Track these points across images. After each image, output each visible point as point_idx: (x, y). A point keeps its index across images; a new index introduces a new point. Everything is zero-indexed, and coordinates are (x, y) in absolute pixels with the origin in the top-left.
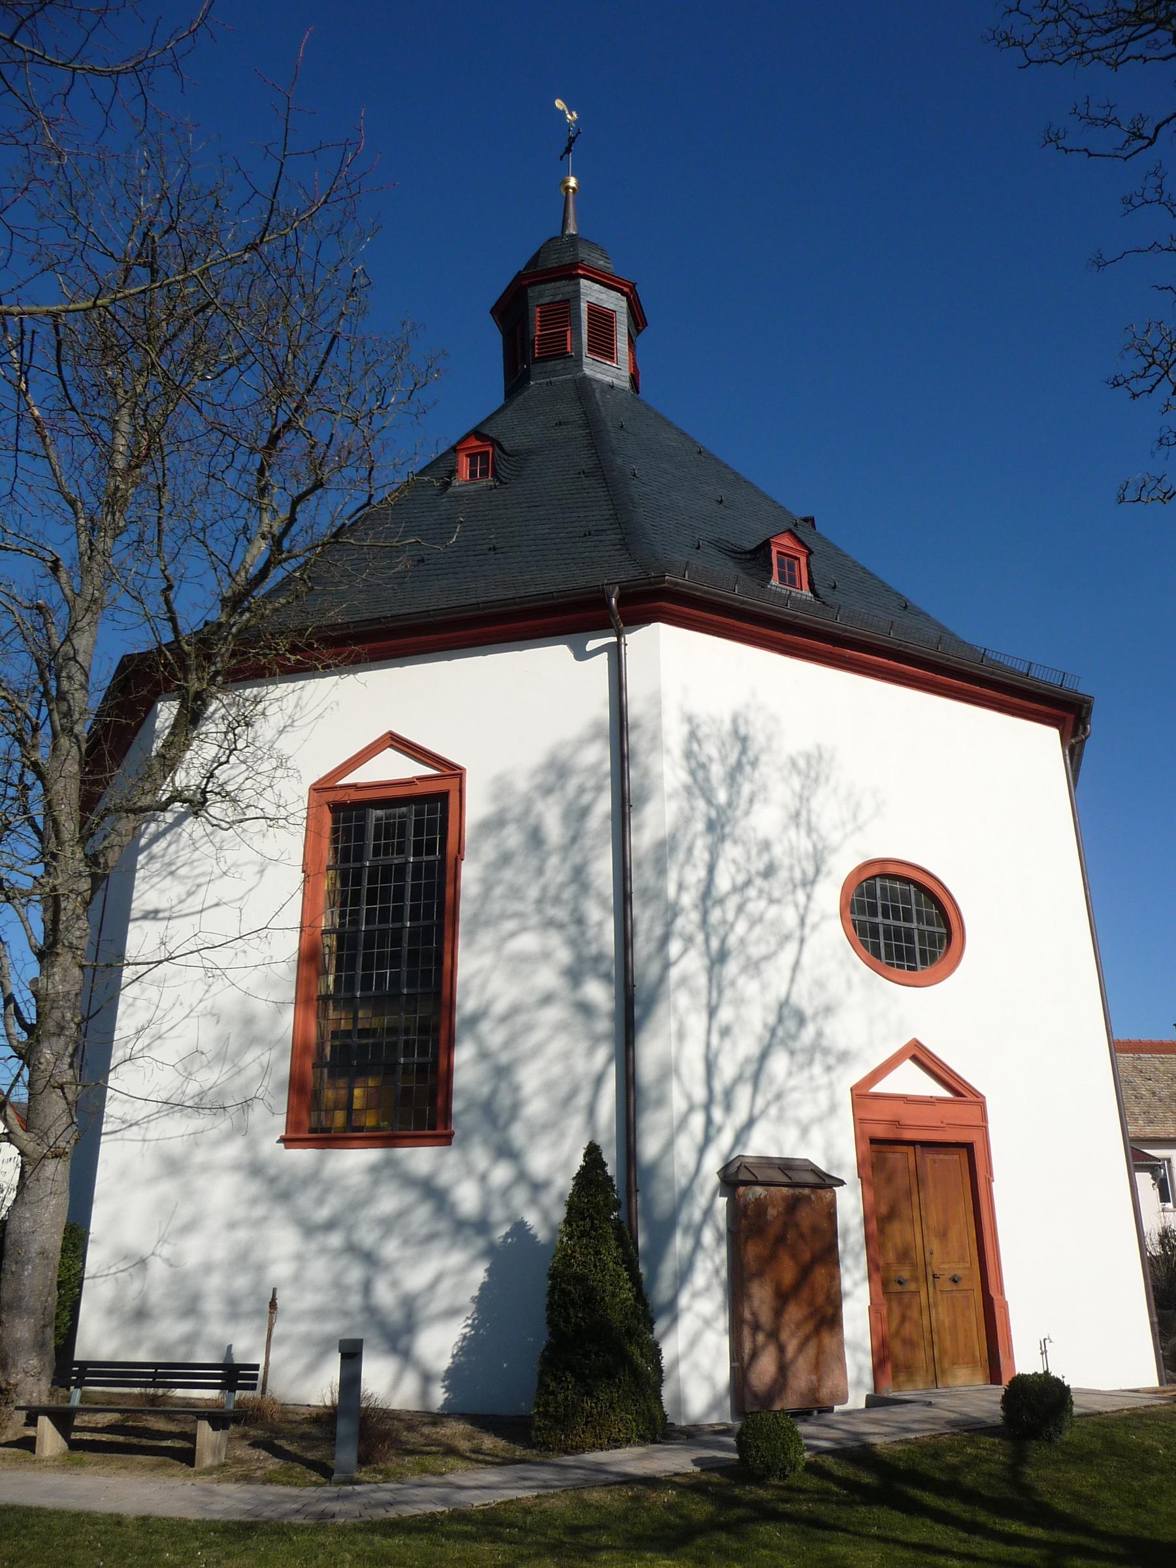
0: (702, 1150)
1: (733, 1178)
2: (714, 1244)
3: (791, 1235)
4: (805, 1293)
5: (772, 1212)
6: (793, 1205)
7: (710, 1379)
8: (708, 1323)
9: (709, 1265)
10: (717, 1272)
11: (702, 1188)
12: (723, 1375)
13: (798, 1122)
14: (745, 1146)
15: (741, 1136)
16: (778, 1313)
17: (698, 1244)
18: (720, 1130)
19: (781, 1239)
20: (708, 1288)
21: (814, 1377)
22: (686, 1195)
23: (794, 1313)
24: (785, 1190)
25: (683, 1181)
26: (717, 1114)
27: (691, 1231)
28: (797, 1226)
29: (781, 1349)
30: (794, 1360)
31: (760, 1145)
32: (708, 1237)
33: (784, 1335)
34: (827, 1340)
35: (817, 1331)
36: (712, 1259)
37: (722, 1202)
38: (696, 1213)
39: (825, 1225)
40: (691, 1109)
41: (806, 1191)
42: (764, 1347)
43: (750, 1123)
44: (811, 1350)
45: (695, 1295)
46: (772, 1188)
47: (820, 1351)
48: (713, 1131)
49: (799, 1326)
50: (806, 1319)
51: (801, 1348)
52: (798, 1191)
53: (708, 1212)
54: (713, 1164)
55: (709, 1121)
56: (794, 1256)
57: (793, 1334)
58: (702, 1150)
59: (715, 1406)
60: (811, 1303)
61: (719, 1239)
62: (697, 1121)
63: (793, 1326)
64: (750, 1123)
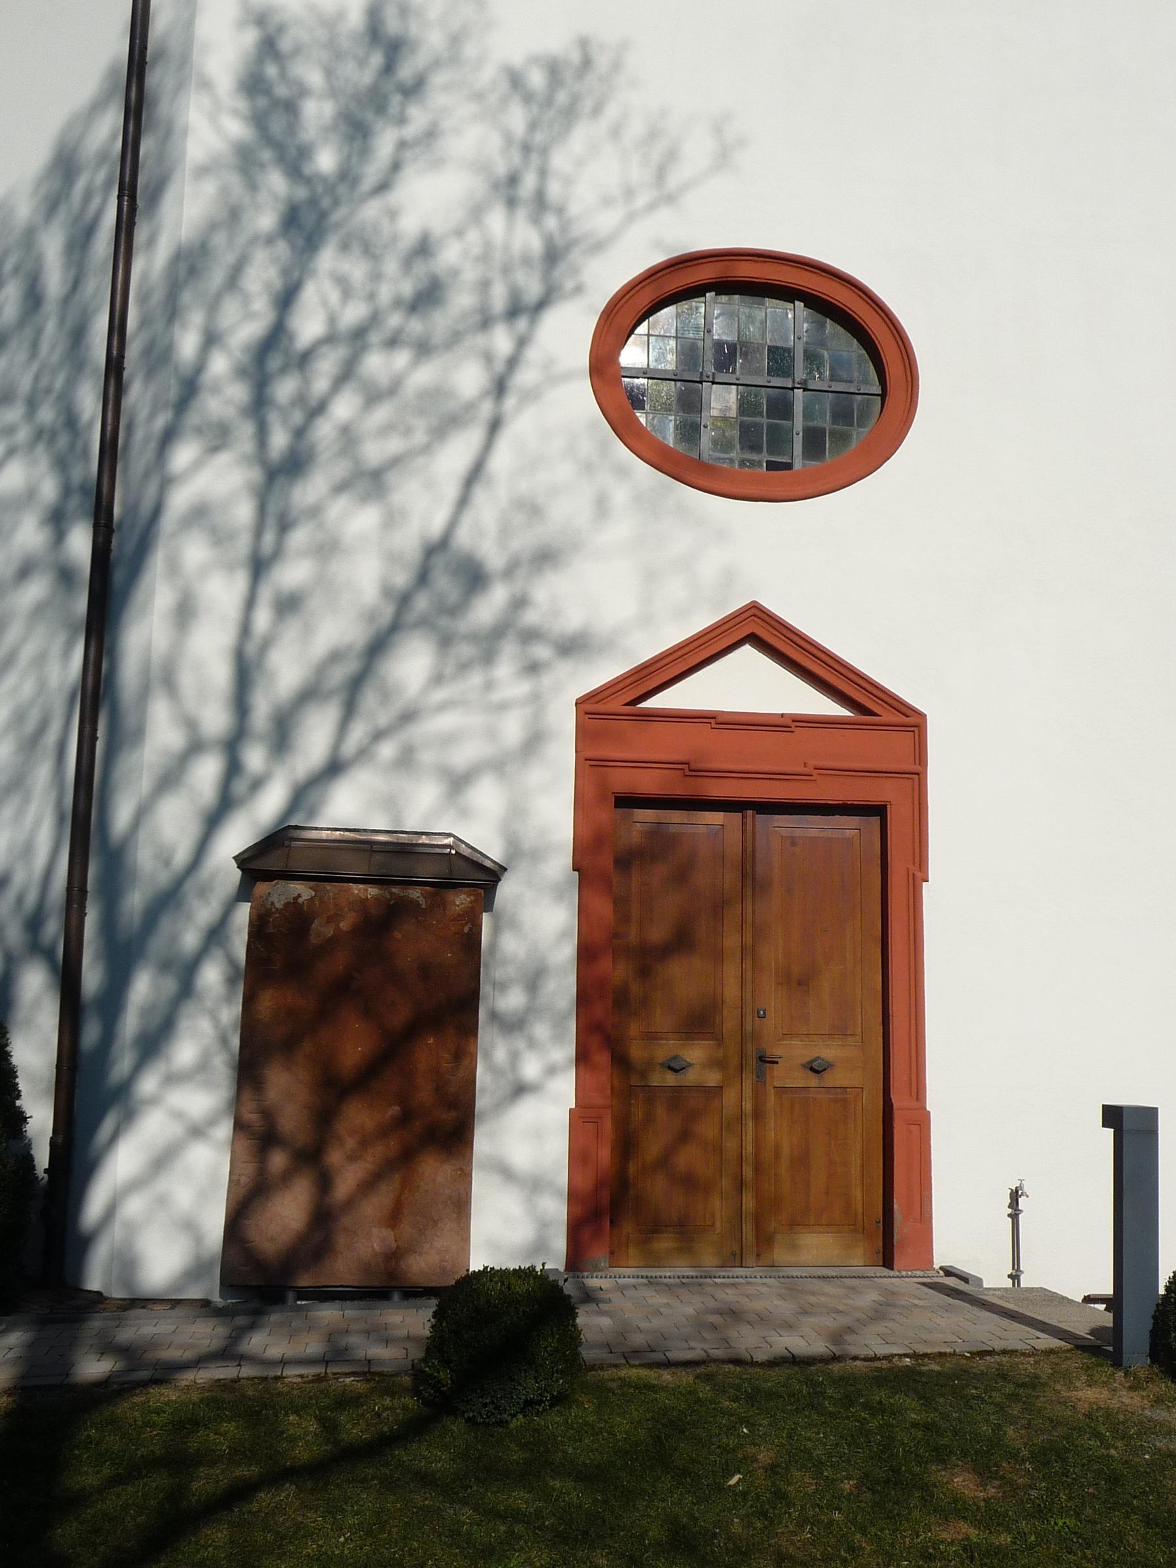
0: (214, 820)
8: (197, 1132)
15: (305, 794)
16: (324, 1119)
17: (186, 989)
18: (257, 784)
20: (202, 1067)
22: (169, 899)
23: (359, 1116)
29: (324, 1183)
30: (350, 1204)
32: (212, 975)
33: (334, 1157)
40: (195, 747)
42: (286, 1177)
45: (172, 1079)
48: (240, 787)
53: (216, 934)
55: (233, 768)
57: (352, 1158)
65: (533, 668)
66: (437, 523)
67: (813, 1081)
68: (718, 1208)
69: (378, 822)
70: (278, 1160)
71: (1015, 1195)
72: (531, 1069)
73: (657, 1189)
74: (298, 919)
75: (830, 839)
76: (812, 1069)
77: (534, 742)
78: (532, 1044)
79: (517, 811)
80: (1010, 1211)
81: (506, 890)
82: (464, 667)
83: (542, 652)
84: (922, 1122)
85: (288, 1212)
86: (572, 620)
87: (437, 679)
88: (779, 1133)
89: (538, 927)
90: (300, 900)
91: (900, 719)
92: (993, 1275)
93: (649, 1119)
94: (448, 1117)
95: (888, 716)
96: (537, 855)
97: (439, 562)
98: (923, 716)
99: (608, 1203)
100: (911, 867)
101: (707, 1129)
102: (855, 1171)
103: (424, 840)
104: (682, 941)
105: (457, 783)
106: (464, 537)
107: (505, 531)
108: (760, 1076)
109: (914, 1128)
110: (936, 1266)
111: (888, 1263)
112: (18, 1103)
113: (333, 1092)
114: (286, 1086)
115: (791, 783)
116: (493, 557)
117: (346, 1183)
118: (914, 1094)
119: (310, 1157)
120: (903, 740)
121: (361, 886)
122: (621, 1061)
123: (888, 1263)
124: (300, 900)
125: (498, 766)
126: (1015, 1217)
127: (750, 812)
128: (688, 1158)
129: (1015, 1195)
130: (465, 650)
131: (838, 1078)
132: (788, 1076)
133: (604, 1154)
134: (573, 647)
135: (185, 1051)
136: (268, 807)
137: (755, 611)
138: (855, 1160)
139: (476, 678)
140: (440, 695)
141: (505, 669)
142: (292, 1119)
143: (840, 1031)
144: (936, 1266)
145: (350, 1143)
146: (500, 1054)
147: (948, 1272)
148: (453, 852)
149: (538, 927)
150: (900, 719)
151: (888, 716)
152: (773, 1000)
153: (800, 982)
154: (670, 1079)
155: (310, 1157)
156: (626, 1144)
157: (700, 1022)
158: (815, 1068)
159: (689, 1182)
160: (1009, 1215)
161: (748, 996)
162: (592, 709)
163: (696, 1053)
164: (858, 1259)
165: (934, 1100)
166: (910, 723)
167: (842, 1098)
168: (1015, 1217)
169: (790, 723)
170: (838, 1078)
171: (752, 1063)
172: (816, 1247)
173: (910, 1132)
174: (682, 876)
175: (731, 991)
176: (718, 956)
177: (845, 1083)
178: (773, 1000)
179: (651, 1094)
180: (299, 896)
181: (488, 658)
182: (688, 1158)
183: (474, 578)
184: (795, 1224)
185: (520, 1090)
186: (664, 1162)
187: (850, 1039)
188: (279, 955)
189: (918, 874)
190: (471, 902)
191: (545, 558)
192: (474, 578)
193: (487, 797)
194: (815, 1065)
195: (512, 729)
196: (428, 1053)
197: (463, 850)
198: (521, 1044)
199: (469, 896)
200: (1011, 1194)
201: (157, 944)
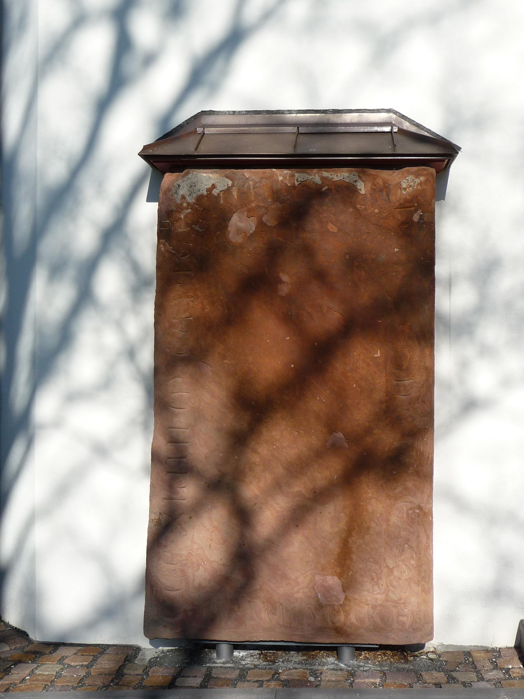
0: (103, 105)
1: (168, 156)
2: (125, 299)
3: (287, 278)
4: (318, 401)
5: (240, 224)
6: (296, 210)
7: (102, 560)
8: (101, 451)
9: (111, 340)
10: (131, 353)
11: (100, 187)
12: (131, 556)
13: (365, 28)
14: (214, 88)
15: (201, 73)
16: (240, 440)
17: (85, 296)
18: (150, 60)
19: (257, 283)
20: (107, 384)
21: (333, 581)
22: (61, 198)
23: (282, 441)
24: (281, 175)
25: (56, 171)
26: (145, 27)
27: (71, 273)
28: (308, 251)
29: (243, 516)
30: (271, 544)
31: (263, 83)
32: (110, 282)
33: (251, 490)
34: (380, 505)
35: (349, 479)
36: (119, 325)
37: (146, 214)
38: (82, 233)
39: (392, 249)
40: (79, 21)
41: (341, 175)
42: (197, 509)
43: (233, 40)
44: (329, 521)
45: (73, 397)
46: (247, 173)
47: (355, 527)
48: (131, 64)
49: (297, 468)
50: (319, 455)
51: (298, 516)
52: (315, 176)
53: (114, 233)
54: (130, 131)
55: (123, 44)
56: (291, 319)
57: (278, 486)
58: (103, 105)
59: (110, 611)
60: (331, 425)
61: (136, 291)
62: (95, 47)
63: (280, 470)
64: (233, 40)
69: (290, 99)
70: (188, 491)
72: (483, 380)
74: (210, 215)
78: (486, 351)
81: (457, 169)
85: (203, 547)
90: (215, 192)
94: (387, 440)
96: (480, 123)
103: (348, 118)
105: (383, 46)
113: (253, 410)
114: (204, 402)
117: (268, 518)
119: (224, 485)
121: (286, 171)
124: (215, 192)
135: (84, 364)
136: (157, 90)
142: (205, 447)
145: (267, 478)
146: (370, 665)
148: (395, 130)
155: (224, 485)
180: (214, 186)
185: (470, 406)
188: (189, 251)
190: (420, 184)
196: (364, 362)
197: (406, 126)
198: (470, 351)
199: (417, 175)
201: (48, 246)
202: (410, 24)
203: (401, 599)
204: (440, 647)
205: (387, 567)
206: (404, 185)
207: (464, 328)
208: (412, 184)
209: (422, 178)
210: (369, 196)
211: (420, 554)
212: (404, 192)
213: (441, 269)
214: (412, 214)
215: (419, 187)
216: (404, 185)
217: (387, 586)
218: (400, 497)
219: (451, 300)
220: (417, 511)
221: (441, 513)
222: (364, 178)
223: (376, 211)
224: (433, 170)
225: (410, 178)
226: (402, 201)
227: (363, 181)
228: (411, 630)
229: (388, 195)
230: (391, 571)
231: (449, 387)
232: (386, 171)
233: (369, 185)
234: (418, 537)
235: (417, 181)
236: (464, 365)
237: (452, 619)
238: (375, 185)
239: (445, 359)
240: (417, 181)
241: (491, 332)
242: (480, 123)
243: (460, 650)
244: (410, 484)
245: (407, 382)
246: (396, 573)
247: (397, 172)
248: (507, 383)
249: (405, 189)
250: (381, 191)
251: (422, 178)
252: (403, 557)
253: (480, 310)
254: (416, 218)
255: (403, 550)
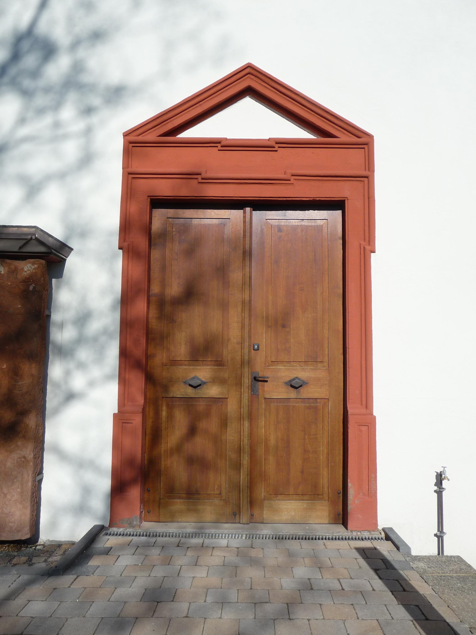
65: (88, 111)
66: (25, 20)
67: (293, 394)
68: (219, 480)
71: (440, 478)
72: (78, 382)
73: (176, 468)
75: (307, 227)
76: (292, 386)
77: (86, 160)
78: (81, 366)
79: (71, 206)
80: (436, 488)
81: (72, 262)
82: (41, 112)
83: (96, 101)
84: (370, 424)
86: (114, 76)
87: (22, 121)
88: (268, 429)
89: (91, 286)
91: (355, 139)
92: (421, 544)
93: (170, 416)
95: (344, 137)
96: (84, 234)
97: (25, 45)
98: (370, 137)
99: (143, 475)
100: (362, 242)
101: (211, 425)
102: (322, 458)
104: (190, 295)
106: (42, 28)
107: (70, 20)
108: (254, 391)
109: (364, 429)
110: (380, 528)
111: (345, 524)
112: (117, 412)
115: (275, 186)
116: (59, 33)
118: (364, 402)
120: (356, 155)
122: (150, 379)
123: (345, 524)
125: (62, 176)
126: (439, 493)
127: (248, 209)
128: (201, 445)
129: (440, 478)
130: (40, 100)
131: (309, 392)
132: (275, 391)
133: (135, 445)
134: (116, 94)
137: (250, 70)
138: (323, 449)
139: (48, 120)
140: (24, 131)
141: (68, 113)
143: (313, 359)
144: (380, 528)
147: (389, 536)
149: (91, 286)
150: (355, 139)
151: (344, 137)
152: (263, 337)
153: (280, 323)
154: (190, 392)
156: (154, 435)
157: (204, 350)
158: (295, 385)
159: (196, 462)
160: (435, 491)
161: (246, 335)
162: (135, 142)
163: (203, 373)
164: (320, 520)
165: (380, 408)
166: (361, 142)
167: (313, 405)
168: (439, 493)
169: (273, 144)
170: (309, 392)
171: (247, 381)
172: (287, 512)
173: (361, 431)
174: (191, 251)
175: (234, 333)
176: (224, 306)
177: (316, 395)
178: (263, 337)
179: (172, 402)
181: (57, 106)
182: (201, 445)
183: (48, 50)
184: (279, 492)
185: (70, 397)
186: (178, 449)
187: (320, 365)
189: (368, 248)
190: (35, 269)
191: (97, 36)
192: (48, 50)
193: (53, 197)
194: (293, 383)
195: (71, 150)
198: (72, 365)
199: (33, 264)
200: (437, 476)
202: (48, 178)
203: (10, 512)
204: (47, 542)
205: (3, 493)
206: (26, 270)
207: (65, 352)
208: (30, 269)
209: (36, 266)
210: (6, 275)
211: (23, 485)
212: (25, 273)
213: (56, 317)
214: (29, 285)
215: (34, 271)
216: (26, 270)
217: (3, 505)
218: (14, 451)
219: (61, 335)
220: (22, 459)
221: (49, 461)
222: (4, 265)
223: (9, 284)
224: (43, 262)
225: (29, 265)
226: (24, 278)
227: (3, 266)
228: (15, 531)
229: (16, 274)
230: (5, 495)
231: (57, 385)
232: (18, 261)
233: (7, 269)
234: (22, 475)
235: (33, 267)
236: (68, 373)
237: (53, 524)
238: (10, 269)
239: (56, 370)
240: (33, 267)
241: (83, 354)
242: (84, 234)
243: (53, 543)
244: (19, 443)
245: (20, 383)
246: (9, 497)
247: (24, 262)
248: (92, 384)
249: (26, 272)
250: (13, 272)
251: (36, 266)
252: (13, 487)
253: (80, 340)
254: (31, 288)
255: (13, 482)
